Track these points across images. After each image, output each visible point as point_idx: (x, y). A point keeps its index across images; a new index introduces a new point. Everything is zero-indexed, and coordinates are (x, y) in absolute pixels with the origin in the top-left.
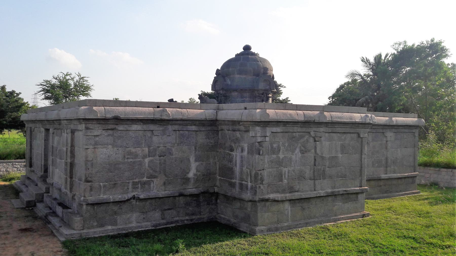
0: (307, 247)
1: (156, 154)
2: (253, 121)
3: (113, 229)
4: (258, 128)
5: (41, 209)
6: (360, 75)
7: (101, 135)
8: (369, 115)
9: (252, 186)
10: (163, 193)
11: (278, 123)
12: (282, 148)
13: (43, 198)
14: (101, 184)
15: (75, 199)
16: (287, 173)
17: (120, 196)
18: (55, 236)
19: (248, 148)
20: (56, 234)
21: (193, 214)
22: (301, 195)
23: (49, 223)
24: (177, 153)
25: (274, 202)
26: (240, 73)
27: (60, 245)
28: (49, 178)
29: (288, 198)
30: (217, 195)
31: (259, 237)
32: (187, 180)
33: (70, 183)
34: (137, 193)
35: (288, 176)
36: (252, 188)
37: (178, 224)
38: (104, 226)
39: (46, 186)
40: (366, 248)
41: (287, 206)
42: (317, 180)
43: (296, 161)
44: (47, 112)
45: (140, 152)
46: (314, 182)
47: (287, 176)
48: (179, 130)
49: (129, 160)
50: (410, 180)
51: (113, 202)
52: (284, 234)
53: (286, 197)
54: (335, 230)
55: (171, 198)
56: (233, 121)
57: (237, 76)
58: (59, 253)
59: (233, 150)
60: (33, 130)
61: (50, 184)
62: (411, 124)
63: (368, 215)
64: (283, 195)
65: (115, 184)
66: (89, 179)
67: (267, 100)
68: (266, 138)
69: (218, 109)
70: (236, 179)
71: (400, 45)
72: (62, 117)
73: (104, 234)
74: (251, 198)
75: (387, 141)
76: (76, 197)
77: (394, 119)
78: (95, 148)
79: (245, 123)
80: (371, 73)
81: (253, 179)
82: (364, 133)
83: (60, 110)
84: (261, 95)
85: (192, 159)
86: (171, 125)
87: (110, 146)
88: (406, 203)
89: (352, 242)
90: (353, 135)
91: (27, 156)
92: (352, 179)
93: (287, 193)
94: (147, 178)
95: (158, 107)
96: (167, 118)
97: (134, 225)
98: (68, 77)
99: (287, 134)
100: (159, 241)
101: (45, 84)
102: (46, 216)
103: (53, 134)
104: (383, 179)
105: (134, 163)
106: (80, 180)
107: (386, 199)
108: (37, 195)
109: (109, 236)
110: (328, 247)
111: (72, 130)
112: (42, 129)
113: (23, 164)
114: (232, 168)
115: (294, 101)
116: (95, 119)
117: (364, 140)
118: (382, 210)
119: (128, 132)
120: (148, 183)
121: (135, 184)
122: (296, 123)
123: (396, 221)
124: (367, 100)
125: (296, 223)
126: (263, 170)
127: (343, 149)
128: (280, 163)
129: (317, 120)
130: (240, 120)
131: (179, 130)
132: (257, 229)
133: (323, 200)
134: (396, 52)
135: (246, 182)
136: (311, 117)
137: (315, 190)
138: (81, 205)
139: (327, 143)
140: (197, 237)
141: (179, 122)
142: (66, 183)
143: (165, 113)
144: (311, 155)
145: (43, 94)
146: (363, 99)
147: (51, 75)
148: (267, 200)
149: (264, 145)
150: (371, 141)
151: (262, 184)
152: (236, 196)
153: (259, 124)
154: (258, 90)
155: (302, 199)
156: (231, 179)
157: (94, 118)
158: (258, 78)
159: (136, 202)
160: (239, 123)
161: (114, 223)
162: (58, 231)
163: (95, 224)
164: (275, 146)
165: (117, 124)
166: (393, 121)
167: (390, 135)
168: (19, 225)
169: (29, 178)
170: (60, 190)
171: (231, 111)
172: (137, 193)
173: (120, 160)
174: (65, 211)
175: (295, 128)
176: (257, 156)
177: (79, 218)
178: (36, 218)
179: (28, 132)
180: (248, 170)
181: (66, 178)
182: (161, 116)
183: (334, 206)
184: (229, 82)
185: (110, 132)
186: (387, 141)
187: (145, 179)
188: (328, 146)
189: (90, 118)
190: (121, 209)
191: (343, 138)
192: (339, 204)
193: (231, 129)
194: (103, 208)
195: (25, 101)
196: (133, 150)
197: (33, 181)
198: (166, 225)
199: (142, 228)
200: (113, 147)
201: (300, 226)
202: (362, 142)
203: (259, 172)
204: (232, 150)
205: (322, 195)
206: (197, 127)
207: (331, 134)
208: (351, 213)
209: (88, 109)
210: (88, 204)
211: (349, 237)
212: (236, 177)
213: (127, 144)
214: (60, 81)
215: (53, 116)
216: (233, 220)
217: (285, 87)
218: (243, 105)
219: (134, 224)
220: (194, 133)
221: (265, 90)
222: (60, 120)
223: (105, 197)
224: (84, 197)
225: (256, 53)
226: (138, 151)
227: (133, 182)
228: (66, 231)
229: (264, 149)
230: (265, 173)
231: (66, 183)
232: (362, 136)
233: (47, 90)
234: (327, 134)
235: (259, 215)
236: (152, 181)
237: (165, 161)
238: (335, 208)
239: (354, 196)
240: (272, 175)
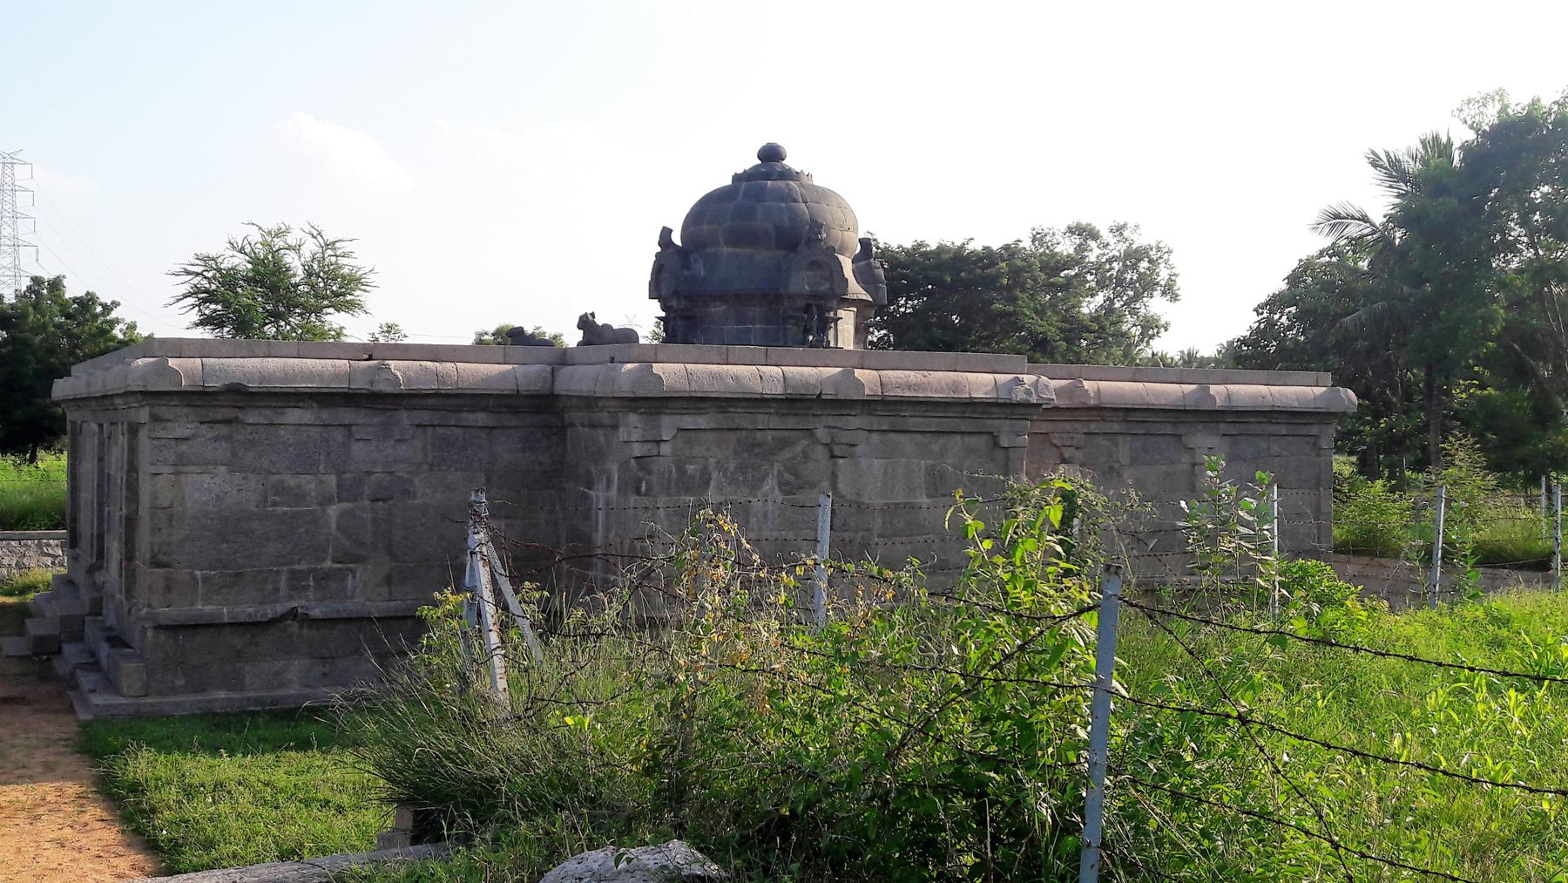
4: (633, 418)
7: (194, 436)
11: (696, 402)
12: (715, 474)
14: (198, 573)
26: (736, 238)
34: (303, 602)
43: (765, 516)
45: (312, 486)
51: (231, 624)
56: (588, 398)
57: (726, 250)
62: (1295, 405)
65: (238, 575)
66: (162, 557)
68: (663, 445)
75: (1194, 465)
77: (1215, 389)
87: (223, 469)
90: (974, 439)
96: (389, 389)
98: (279, 243)
99: (732, 436)
101: (200, 269)
105: (294, 516)
120: (340, 576)
121: (294, 575)
129: (829, 393)
136: (807, 385)
141: (430, 401)
145: (194, 306)
147: (225, 237)
149: (654, 467)
150: (1125, 460)
153: (634, 404)
154: (791, 297)
159: (301, 627)
161: (236, 683)
163: (181, 682)
164: (691, 468)
166: (1213, 397)
172: (303, 602)
173: (253, 508)
182: (372, 383)
185: (223, 430)
187: (328, 564)
191: (936, 447)
196: (291, 481)
202: (1007, 458)
207: (892, 435)
210: (158, 628)
214: (256, 261)
219: (293, 691)
221: (815, 295)
223: (208, 608)
224: (150, 606)
226: (308, 483)
229: (654, 478)
232: (1004, 442)
234: (875, 437)
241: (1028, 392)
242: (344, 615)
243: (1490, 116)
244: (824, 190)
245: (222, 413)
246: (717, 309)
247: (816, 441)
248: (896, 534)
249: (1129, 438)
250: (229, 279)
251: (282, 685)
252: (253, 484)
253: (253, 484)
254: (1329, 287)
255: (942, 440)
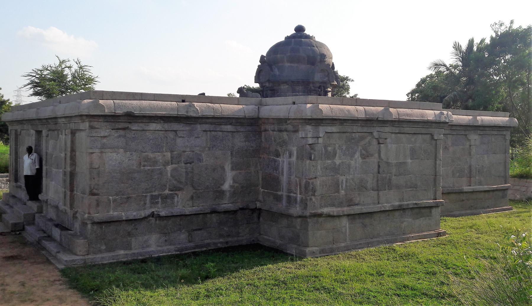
0: (366, 269)
1: (181, 161)
2: (302, 119)
3: (127, 254)
4: (309, 128)
5: (31, 233)
6: (445, 65)
7: (109, 135)
8: (445, 112)
9: (302, 198)
10: (190, 209)
11: (333, 121)
12: (338, 151)
13: (34, 219)
14: (111, 197)
15: (77, 218)
16: (344, 182)
17: (135, 213)
18: (50, 263)
19: (297, 153)
20: (52, 261)
21: (228, 236)
22: (362, 209)
23: (44, 249)
24: (208, 159)
25: (328, 218)
26: (291, 60)
27: (59, 274)
28: (42, 194)
29: (346, 213)
30: (258, 211)
31: (309, 260)
32: (221, 194)
33: (70, 197)
34: (157, 209)
35: (346, 186)
36: (302, 200)
37: (210, 248)
38: (114, 251)
39: (38, 204)
40: (436, 269)
41: (345, 222)
42: (381, 190)
43: (356, 168)
44: (38, 109)
45: (160, 158)
46: (378, 194)
47: (344, 186)
48: (210, 131)
49: (147, 168)
50: (500, 194)
51: (126, 220)
52: (340, 255)
53: (343, 211)
54: (402, 250)
55: (201, 216)
57: (287, 64)
58: (58, 283)
59: (280, 155)
60: (19, 133)
61: (44, 201)
62: (501, 124)
63: (444, 234)
64: (339, 209)
65: (128, 198)
67: (326, 94)
68: (319, 139)
69: (260, 104)
70: (283, 191)
71: (501, 25)
72: (59, 114)
73: (115, 261)
74: (300, 213)
75: (470, 146)
76: (78, 215)
77: (478, 118)
78: (102, 152)
79: (293, 121)
80: (460, 64)
81: (303, 189)
82: (439, 134)
83: (56, 106)
84: (318, 89)
85: (228, 167)
86: (200, 124)
87: (122, 150)
88: (493, 220)
89: (420, 262)
91: (10, 169)
92: (425, 190)
93: (345, 206)
94: (171, 190)
95: (183, 101)
97: (152, 249)
99: (344, 135)
100: (185, 266)
101: (34, 75)
102: (39, 242)
103: (47, 136)
104: (466, 192)
105: (153, 171)
106: (84, 193)
107: (469, 217)
108: (25, 216)
109: (121, 262)
110: (391, 269)
111: (72, 130)
112: (32, 131)
113: (5, 179)
114: (278, 178)
115: (362, 96)
116: (102, 116)
117: (438, 143)
118: (461, 228)
119: (144, 132)
120: (172, 197)
121: (153, 197)
122: (355, 121)
123: (477, 241)
124: (455, 96)
125: (356, 243)
126: (316, 178)
127: (413, 152)
128: (336, 170)
129: (381, 117)
130: (287, 117)
131: (210, 131)
132: (308, 250)
133: (389, 215)
134: (494, 35)
135: (295, 193)
136: (373, 114)
137: (379, 203)
138: (84, 224)
139: (394, 146)
140: (233, 262)
141: (210, 120)
142: (65, 198)
143: (192, 109)
144: (374, 160)
145: (31, 88)
146: (451, 95)
147: (47, 60)
148: (320, 215)
150: (450, 144)
151: (314, 195)
152: (283, 213)
153: (310, 122)
154: (313, 83)
155: (363, 214)
156: (277, 191)
157: (100, 114)
158: (313, 67)
159: (156, 220)
160: (286, 122)
161: (128, 247)
162: (55, 257)
163: (103, 247)
164: (329, 149)
165: (130, 123)
167: (474, 137)
168: (4, 252)
169: (14, 197)
170: (57, 207)
171: (277, 107)
173: (135, 168)
174: (64, 232)
175: (355, 127)
176: (308, 162)
177: (82, 241)
178: (25, 243)
179: (12, 137)
180: (298, 179)
181: (65, 192)
183: (402, 223)
184: (276, 72)
185: (122, 132)
186: (470, 146)
187: (167, 192)
188: (394, 149)
189: (95, 114)
190: (137, 229)
191: (413, 140)
192: (408, 221)
193: (276, 129)
194: (112, 227)
195: (5, 98)
196: (151, 155)
197: (20, 200)
198: (194, 248)
199: (163, 253)
200: (125, 151)
201: (359, 246)
202: (436, 144)
203: (311, 181)
204: (278, 155)
205: (388, 209)
206: (234, 127)
207: (399, 135)
208: (422, 232)
209: (93, 102)
210: (94, 223)
211: (417, 258)
212: (283, 189)
213: (143, 147)
214: (54, 72)
215: (47, 112)
216: (279, 242)
217: (352, 81)
218: (290, 99)
219: (153, 248)
220: (230, 134)
222: (56, 118)
223: (116, 213)
224: (89, 213)
225: (311, 35)
226: (158, 156)
227: (152, 196)
228: (65, 257)
230: (318, 182)
231: (65, 198)
232: (436, 138)
233: (36, 83)
234: (393, 135)
235: (310, 233)
236: (176, 194)
237: (193, 169)
238: (403, 226)
239: (427, 210)
240: (326, 185)
241: (445, 118)
242: (175, 214)
243: (503, 29)
244: (320, 43)
245: (122, 125)
246: (284, 87)
247: (373, 137)
248: (400, 175)
249: (451, 136)
250: (42, 78)
251: (148, 246)
252: (135, 157)
253: (135, 157)
254: (151, 108)
255: (415, 136)
